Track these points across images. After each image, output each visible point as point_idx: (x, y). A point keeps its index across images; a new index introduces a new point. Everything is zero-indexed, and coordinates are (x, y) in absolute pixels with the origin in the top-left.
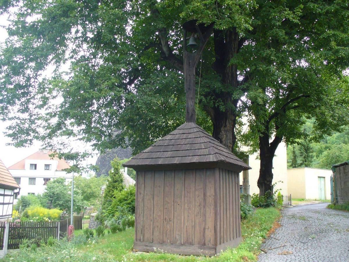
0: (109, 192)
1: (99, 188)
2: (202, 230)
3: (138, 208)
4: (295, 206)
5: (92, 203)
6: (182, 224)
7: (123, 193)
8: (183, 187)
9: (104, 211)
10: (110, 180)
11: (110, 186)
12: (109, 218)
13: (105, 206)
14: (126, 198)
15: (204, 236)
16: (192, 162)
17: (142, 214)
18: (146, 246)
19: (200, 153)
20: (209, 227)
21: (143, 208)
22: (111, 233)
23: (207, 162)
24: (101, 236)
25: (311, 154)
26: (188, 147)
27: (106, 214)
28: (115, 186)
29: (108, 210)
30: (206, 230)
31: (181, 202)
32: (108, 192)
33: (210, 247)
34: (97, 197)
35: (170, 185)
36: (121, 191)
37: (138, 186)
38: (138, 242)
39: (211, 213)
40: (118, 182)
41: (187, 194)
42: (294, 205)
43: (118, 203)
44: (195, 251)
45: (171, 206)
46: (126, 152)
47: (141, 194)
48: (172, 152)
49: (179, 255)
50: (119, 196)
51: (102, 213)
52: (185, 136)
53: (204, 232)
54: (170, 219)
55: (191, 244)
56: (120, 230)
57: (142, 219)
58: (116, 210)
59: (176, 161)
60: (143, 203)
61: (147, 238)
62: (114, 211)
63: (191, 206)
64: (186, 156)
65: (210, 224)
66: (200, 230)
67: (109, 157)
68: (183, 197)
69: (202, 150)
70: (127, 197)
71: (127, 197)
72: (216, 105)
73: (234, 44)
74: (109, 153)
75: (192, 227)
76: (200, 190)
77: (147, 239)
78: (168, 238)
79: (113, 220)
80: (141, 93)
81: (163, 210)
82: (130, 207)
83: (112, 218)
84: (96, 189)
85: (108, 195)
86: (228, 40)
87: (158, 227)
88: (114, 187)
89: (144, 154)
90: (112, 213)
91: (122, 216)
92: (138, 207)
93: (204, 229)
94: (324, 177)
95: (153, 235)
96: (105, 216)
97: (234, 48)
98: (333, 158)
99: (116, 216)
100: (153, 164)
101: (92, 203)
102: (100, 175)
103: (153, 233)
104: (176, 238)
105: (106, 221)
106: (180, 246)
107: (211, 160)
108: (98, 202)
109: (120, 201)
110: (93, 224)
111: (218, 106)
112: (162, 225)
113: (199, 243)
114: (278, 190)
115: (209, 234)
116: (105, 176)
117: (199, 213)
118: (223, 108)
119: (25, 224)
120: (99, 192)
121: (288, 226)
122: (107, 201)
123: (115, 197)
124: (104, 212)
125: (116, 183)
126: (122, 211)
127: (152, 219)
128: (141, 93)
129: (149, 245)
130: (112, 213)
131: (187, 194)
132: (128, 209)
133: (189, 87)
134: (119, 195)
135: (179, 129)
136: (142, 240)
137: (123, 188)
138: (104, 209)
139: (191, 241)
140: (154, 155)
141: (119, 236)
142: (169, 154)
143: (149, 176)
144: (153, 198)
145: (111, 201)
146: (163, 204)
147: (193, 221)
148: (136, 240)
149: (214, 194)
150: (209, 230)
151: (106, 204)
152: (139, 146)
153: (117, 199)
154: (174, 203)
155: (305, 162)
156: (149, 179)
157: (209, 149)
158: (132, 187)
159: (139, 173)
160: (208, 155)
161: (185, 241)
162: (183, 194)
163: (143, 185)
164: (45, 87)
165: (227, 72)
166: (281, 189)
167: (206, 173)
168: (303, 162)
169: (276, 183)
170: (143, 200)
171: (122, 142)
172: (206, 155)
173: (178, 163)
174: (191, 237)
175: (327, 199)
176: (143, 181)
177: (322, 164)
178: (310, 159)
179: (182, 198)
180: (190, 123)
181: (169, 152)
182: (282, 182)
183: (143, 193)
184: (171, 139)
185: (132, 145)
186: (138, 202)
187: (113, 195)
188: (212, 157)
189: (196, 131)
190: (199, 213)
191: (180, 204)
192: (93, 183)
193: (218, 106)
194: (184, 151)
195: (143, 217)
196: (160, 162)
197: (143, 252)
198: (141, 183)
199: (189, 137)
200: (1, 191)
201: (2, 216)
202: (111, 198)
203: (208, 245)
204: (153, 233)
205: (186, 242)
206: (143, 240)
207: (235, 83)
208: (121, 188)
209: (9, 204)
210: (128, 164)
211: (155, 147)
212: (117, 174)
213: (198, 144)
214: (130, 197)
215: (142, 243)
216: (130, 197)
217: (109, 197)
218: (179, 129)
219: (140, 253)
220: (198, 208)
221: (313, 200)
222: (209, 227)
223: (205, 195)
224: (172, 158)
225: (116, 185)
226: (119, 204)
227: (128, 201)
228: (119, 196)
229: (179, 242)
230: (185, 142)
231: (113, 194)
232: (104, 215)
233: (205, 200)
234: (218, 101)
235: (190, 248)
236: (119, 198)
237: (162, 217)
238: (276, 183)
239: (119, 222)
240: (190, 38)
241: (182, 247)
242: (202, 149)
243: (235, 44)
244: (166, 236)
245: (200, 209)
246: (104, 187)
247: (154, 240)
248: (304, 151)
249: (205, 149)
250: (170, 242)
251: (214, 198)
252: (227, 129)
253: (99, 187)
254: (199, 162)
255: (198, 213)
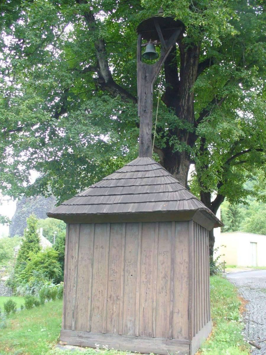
0: (24, 253)
1: (12, 249)
2: (168, 314)
3: (68, 280)
4: (228, 274)
5: (4, 265)
6: (137, 305)
7: (39, 254)
8: (139, 247)
9: (17, 275)
10: (25, 239)
11: (24, 247)
12: (22, 284)
13: (18, 269)
14: (43, 261)
15: (171, 323)
16: (157, 210)
17: (75, 288)
18: (80, 337)
19: (168, 197)
20: (178, 310)
21: (76, 280)
22: (25, 308)
23: (181, 211)
24: (11, 313)
25: (238, 219)
26: (146, 189)
27: (20, 278)
28: (30, 246)
29: (21, 274)
30: (175, 315)
31: (135, 271)
32: (22, 253)
33: (180, 341)
34: (10, 258)
35: (118, 245)
36: (38, 253)
37: (69, 246)
38: (68, 331)
39: (182, 289)
40: (34, 242)
41: (146, 260)
42: (227, 272)
43: (34, 267)
44: (156, 347)
45: (120, 278)
46: (42, 212)
47: (74, 258)
48: (122, 196)
49: (132, 352)
50: (35, 259)
51: (14, 278)
52: (140, 175)
53: (172, 318)
54: (117, 297)
55: (151, 336)
56: (37, 304)
57: (75, 296)
58: (31, 275)
59: (131, 209)
60: (76, 271)
61: (82, 325)
62: (28, 276)
63: (152, 278)
64: (146, 202)
65: (181, 305)
66: (165, 315)
67: (24, 217)
68: (139, 264)
69: (170, 193)
70: (44, 260)
71: (44, 260)
72: (170, 144)
73: (192, 70)
74: (24, 213)
75: (153, 310)
76: (165, 253)
77: (81, 326)
78: (114, 326)
79: (27, 286)
80: (74, 121)
81: (107, 282)
82: (47, 272)
83: (25, 283)
84: (8, 250)
85: (22, 256)
86: (185, 65)
87: (98, 308)
88: (29, 248)
89: (80, 198)
90: (26, 278)
91: (38, 281)
92: (68, 276)
93: (172, 313)
94: (256, 243)
95: (91, 320)
96: (17, 281)
97: (192, 75)
98: (258, 224)
99: (30, 281)
100: (95, 213)
101: (4, 265)
102: (14, 235)
103: (91, 317)
104: (126, 326)
105: (19, 287)
106: (133, 338)
107: (187, 208)
108: (10, 264)
109: (36, 264)
110: (3, 289)
111: (173, 145)
112: (105, 305)
113: (163, 335)
114: (221, 255)
115: (180, 322)
116: (19, 236)
117: (164, 288)
118: (180, 148)
120: (13, 253)
121: (212, 294)
122: (21, 264)
123: (30, 260)
124: (16, 277)
125: (32, 243)
126: (38, 276)
127: (90, 296)
128: (74, 121)
129: (84, 336)
130: (26, 278)
131: (146, 260)
132: (45, 274)
133: (144, 109)
134: (35, 257)
135: (129, 166)
136: (73, 328)
137: (39, 249)
138: (16, 272)
139: (151, 331)
140: (96, 200)
141: (37, 313)
142: (119, 199)
143: (86, 231)
144: (92, 265)
145: (25, 264)
146: (107, 274)
147: (155, 301)
148: (65, 327)
149: (187, 260)
150: (180, 315)
151: (19, 267)
152: (65, 194)
153: (33, 262)
154: (124, 272)
155: (233, 227)
156: (87, 233)
157: (179, 192)
158: (50, 248)
159: (71, 227)
160: (180, 200)
161: (141, 331)
162: (139, 259)
163: (77, 245)
165: (182, 104)
166: (224, 255)
167: (175, 228)
168: (231, 227)
169: (218, 248)
170: (77, 266)
171: (43, 188)
172: (176, 201)
173: (134, 211)
174: (150, 325)
175: (259, 266)
176: (77, 239)
177: (247, 229)
178: (237, 224)
179: (137, 266)
180: (145, 159)
181: (118, 197)
182: (225, 247)
183: (77, 257)
184: (120, 178)
185: (57, 193)
186: (69, 270)
187: (28, 257)
188: (187, 203)
189: (155, 168)
190: (164, 288)
191: (133, 275)
192: (6, 243)
193: (173, 145)
194: (141, 195)
195: (76, 292)
196: (105, 210)
197: (75, 347)
198: (74, 241)
199: (146, 176)
202: (25, 260)
203: (178, 338)
204: (91, 317)
205: (142, 332)
206: (76, 328)
207: (191, 119)
208: (37, 249)
210: (56, 212)
211: (96, 189)
212: (33, 233)
213: (162, 186)
214: (47, 260)
215: (71, 330)
216: (47, 260)
217: (23, 259)
218: (129, 166)
219: (70, 347)
220: (162, 282)
221: (246, 267)
222: (178, 310)
223: (173, 261)
224: (123, 204)
225: (31, 246)
226: (34, 267)
227: (45, 265)
228: (35, 259)
229: (131, 332)
230: (141, 183)
231: (27, 256)
232: (16, 280)
233: (173, 269)
234: (172, 138)
235: (149, 343)
236: (35, 261)
237: (106, 294)
238: (218, 248)
239: (34, 289)
240: (146, 45)
241: (136, 340)
242: (169, 192)
243: (194, 70)
244: (111, 323)
245: (166, 283)
246: (18, 247)
247: (92, 329)
248: (232, 215)
249: (174, 193)
250: (118, 331)
251: (187, 265)
252: (180, 177)
253: (12, 248)
254: (167, 211)
255: (162, 288)
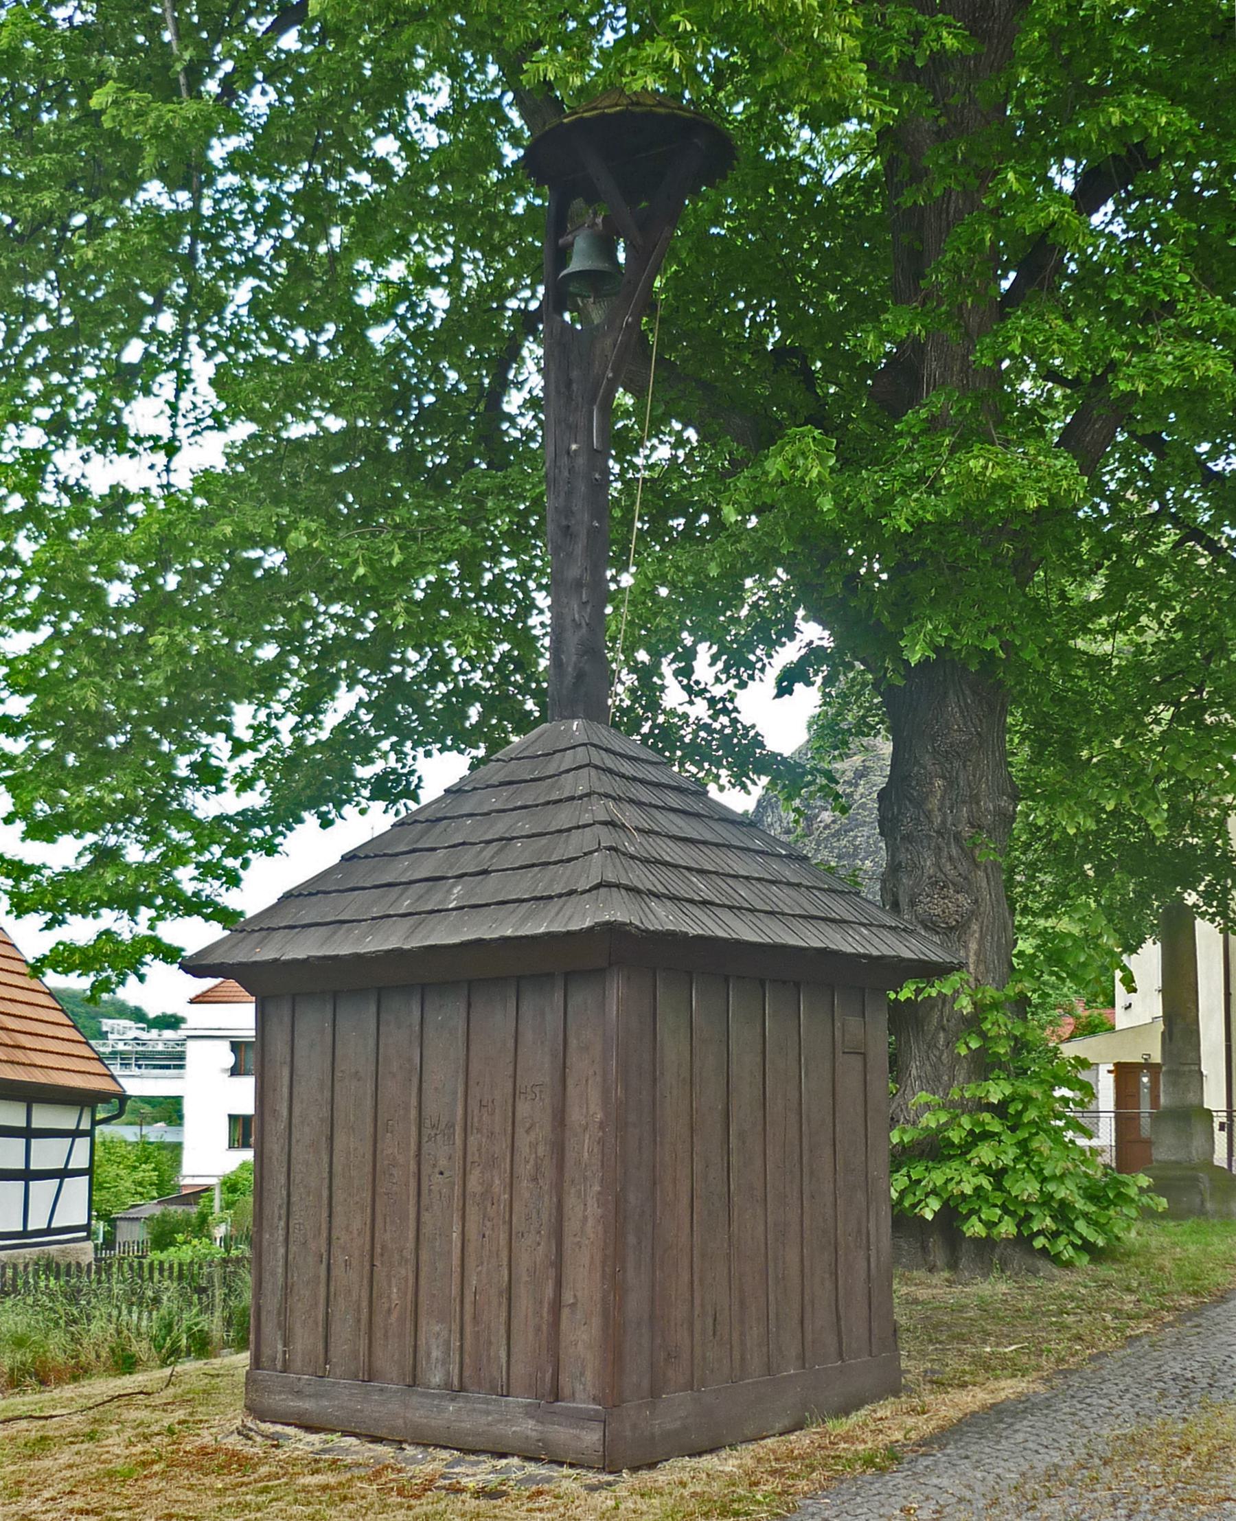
30: (565, 1313)
53: (556, 1323)
117: (534, 1215)
119: (631, 1239)
133: (564, 523)
164: (687, 740)
183: (285, 1113)
200: (12, 1115)
201: (25, 1234)
209: (63, 1174)
235: (488, 1413)
